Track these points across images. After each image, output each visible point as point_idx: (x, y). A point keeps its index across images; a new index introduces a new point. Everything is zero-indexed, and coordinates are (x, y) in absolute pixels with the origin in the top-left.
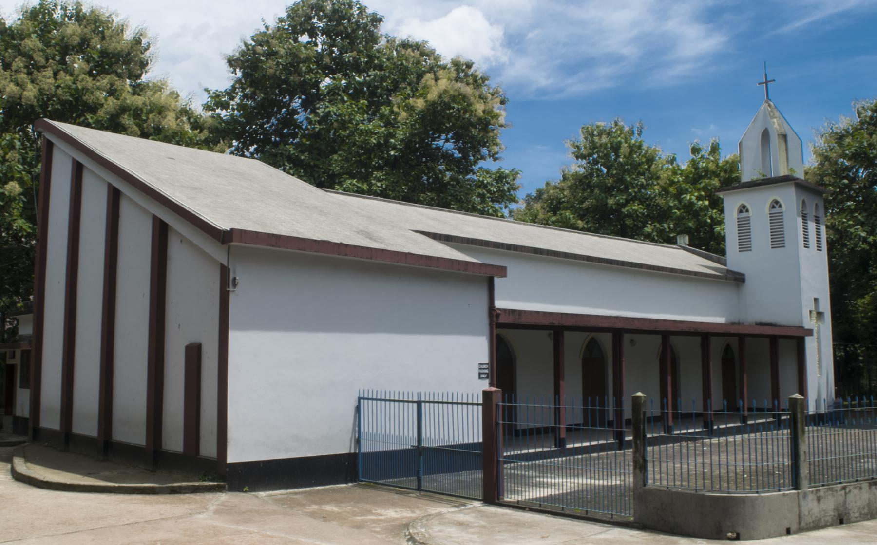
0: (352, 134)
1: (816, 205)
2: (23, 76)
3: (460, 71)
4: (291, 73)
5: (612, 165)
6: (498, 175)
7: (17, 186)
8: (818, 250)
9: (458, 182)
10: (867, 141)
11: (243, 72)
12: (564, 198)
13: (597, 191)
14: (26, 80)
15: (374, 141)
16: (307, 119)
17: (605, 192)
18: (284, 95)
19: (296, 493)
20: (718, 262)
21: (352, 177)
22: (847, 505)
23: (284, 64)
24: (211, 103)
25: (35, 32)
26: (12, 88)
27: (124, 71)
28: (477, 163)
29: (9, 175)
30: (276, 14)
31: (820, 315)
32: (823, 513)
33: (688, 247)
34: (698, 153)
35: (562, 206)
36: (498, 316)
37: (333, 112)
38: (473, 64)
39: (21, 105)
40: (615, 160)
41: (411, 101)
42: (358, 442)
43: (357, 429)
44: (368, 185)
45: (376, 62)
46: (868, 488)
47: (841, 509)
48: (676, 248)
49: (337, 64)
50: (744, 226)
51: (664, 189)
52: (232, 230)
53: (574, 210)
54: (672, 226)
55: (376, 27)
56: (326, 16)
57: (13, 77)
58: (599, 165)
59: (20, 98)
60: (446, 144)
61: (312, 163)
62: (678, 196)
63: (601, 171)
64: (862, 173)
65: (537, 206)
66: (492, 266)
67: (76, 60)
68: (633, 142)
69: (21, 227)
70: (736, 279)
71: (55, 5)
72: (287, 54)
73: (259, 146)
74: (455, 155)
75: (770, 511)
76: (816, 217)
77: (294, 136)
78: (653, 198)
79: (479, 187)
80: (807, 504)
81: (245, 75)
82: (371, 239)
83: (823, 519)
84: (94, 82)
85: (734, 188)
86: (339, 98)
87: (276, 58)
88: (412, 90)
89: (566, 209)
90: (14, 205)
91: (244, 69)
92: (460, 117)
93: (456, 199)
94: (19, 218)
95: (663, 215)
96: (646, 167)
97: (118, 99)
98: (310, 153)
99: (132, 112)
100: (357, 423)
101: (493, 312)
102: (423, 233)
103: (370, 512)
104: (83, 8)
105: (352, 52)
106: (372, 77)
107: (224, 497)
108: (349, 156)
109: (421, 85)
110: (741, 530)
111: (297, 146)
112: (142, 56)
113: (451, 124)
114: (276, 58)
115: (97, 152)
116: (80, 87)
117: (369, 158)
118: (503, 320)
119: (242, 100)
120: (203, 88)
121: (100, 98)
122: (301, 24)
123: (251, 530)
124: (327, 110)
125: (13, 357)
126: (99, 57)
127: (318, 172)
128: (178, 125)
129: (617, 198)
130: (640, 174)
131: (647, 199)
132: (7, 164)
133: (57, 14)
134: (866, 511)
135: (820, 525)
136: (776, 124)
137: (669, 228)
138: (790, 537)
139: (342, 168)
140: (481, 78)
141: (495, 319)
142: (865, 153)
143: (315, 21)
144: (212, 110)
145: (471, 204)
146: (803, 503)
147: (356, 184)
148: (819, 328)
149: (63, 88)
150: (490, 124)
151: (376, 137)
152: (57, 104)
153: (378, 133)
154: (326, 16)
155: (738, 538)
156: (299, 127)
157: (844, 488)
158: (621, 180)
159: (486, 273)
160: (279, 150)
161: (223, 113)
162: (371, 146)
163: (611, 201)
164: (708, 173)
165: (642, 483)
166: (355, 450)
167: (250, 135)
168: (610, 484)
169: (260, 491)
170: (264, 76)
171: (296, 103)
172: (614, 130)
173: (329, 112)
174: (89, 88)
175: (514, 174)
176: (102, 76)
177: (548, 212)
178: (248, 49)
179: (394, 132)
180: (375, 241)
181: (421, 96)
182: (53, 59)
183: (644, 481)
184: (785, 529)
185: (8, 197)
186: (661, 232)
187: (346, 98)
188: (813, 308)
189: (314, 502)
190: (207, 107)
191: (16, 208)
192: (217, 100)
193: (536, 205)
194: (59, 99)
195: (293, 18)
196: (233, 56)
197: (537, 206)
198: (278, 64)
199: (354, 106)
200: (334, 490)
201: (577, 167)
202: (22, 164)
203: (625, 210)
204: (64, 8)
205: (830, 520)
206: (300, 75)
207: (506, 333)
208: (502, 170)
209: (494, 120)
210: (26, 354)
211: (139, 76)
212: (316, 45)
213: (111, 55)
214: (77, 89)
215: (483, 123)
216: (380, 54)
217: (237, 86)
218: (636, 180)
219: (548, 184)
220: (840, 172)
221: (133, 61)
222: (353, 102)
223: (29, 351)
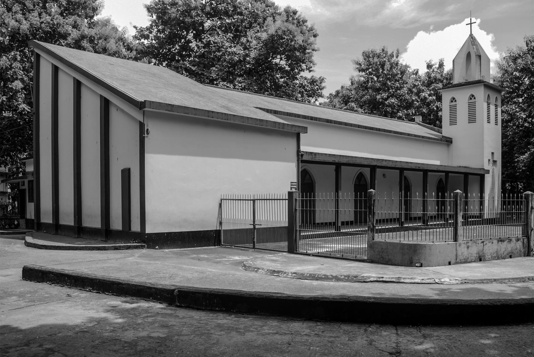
0: (224, 54)
1: (496, 98)
2: (19, 16)
3: (289, 16)
4: (186, 16)
5: (380, 75)
6: (311, 80)
7: (20, 83)
8: (496, 124)
10: (530, 61)
11: (156, 16)
12: (352, 95)
14: (21, 18)
16: (197, 45)
17: (375, 92)
18: (182, 31)
19: (185, 250)
20: (438, 132)
21: (224, 81)
22: (484, 251)
23: (182, 10)
24: (138, 35)
26: (13, 23)
27: (83, 13)
28: (300, 74)
31: (495, 162)
32: (470, 255)
33: (421, 123)
35: (350, 100)
36: (302, 155)
37: (212, 41)
38: (297, 12)
39: (19, 34)
40: (382, 72)
41: (259, 34)
42: (221, 223)
43: (220, 216)
44: (233, 85)
45: (239, 10)
46: (497, 243)
48: (414, 124)
49: (215, 12)
50: (453, 110)
51: (410, 91)
52: (145, 101)
53: (357, 103)
54: (414, 112)
57: (13, 17)
58: (372, 76)
59: (19, 29)
61: (200, 72)
62: (418, 94)
63: (374, 79)
64: (527, 81)
65: (336, 100)
67: (53, 6)
68: (393, 61)
69: (24, 109)
70: (447, 141)
72: (183, 5)
73: (169, 62)
74: (286, 69)
75: (440, 252)
76: (495, 105)
77: (190, 56)
78: (404, 95)
79: (300, 87)
80: (461, 250)
81: (158, 18)
82: (229, 110)
83: (470, 258)
84: (64, 20)
86: (216, 32)
87: (177, 7)
88: (260, 28)
89: (352, 101)
90: (19, 95)
91: (157, 14)
92: (288, 44)
93: (286, 94)
94: (23, 103)
95: (409, 105)
96: (400, 76)
97: (80, 31)
98: (199, 66)
99: (88, 38)
100: (220, 213)
102: (260, 109)
103: (225, 257)
105: (223, 3)
106: (236, 19)
109: (265, 24)
110: (422, 262)
111: (191, 62)
112: (94, 4)
113: (283, 48)
114: (177, 7)
116: (56, 23)
117: (234, 69)
118: (305, 158)
119: (157, 34)
120: (132, 26)
121: (69, 30)
123: (157, 263)
125: (24, 185)
127: (203, 78)
128: (117, 47)
129: (382, 95)
130: (396, 81)
131: (400, 96)
132: (13, 70)
134: (495, 255)
135: (468, 261)
136: (475, 49)
137: (412, 113)
138: (450, 266)
140: (302, 21)
142: (529, 68)
144: (138, 40)
145: (295, 97)
146: (458, 248)
147: (226, 85)
148: (493, 169)
149: (45, 23)
151: (238, 56)
152: (42, 33)
153: (239, 54)
155: (421, 266)
156: (192, 51)
157: (483, 242)
158: (385, 84)
159: (295, 130)
160: (180, 64)
161: (146, 42)
162: (235, 62)
163: (378, 97)
164: (436, 80)
165: (372, 239)
166: (219, 228)
168: (362, 247)
169: (165, 249)
170: (170, 18)
171: (190, 36)
172: (382, 54)
173: (210, 41)
174: (61, 23)
175: (322, 80)
176: (69, 16)
177: (342, 103)
179: (249, 53)
180: (231, 111)
181: (265, 31)
182: (38, 5)
183: (373, 237)
184: (448, 262)
185: (14, 90)
186: (407, 115)
187: (220, 33)
189: (195, 254)
190: (135, 37)
191: (21, 97)
192: (142, 33)
193: (335, 100)
194: (43, 30)
196: (151, 5)
197: (336, 100)
198: (178, 10)
199: (224, 37)
201: (360, 77)
202: (22, 71)
203: (386, 102)
205: (474, 259)
206: (192, 18)
207: (310, 168)
208: (314, 78)
209: (309, 46)
210: (31, 182)
211: (92, 17)
213: (74, 3)
214: (54, 24)
215: (302, 48)
216: (241, 5)
217: (154, 24)
218: (394, 84)
219: (342, 87)
220: (514, 80)
221: (88, 7)
222: (224, 35)
223: (33, 181)
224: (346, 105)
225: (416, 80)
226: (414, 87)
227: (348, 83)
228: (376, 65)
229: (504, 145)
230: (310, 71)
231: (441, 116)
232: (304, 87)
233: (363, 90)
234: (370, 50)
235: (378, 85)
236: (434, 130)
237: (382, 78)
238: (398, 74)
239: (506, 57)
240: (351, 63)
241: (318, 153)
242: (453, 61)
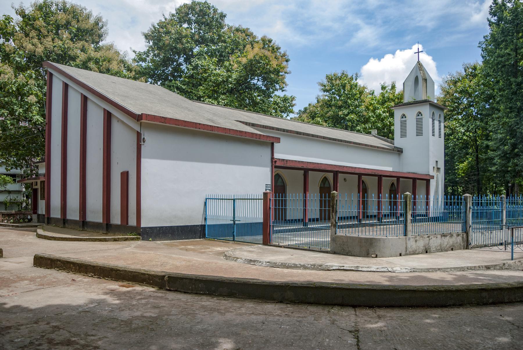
0: (209, 75)
2: (35, 41)
4: (178, 43)
5: (342, 95)
7: (34, 98)
9: (264, 102)
13: (333, 108)
15: (220, 79)
19: (175, 242)
20: (391, 143)
25: (41, 17)
26: (30, 47)
29: (30, 92)
30: (170, 12)
31: (438, 169)
34: (385, 89)
36: (275, 162)
38: (272, 40)
39: (35, 56)
40: (344, 92)
41: (240, 59)
42: (205, 219)
47: (427, 246)
49: (202, 40)
50: (403, 125)
51: (367, 108)
54: (370, 126)
55: (223, 20)
56: (196, 13)
59: (35, 52)
60: (258, 82)
61: (189, 91)
62: (374, 111)
65: (304, 116)
66: (273, 137)
69: (38, 119)
70: (398, 151)
71: (52, 3)
74: (263, 88)
75: (392, 245)
77: (180, 77)
79: (274, 104)
81: (154, 44)
85: (399, 106)
88: (241, 53)
89: (318, 117)
90: (33, 107)
92: (264, 68)
95: (366, 121)
101: (273, 160)
102: (240, 122)
104: (67, 5)
107: (139, 242)
108: (208, 87)
109: (245, 50)
111: (181, 82)
112: (100, 32)
115: (75, 77)
117: (219, 88)
122: (183, 17)
124: (196, 63)
126: (76, 31)
130: (355, 99)
131: (359, 112)
132: (29, 86)
133: (54, 8)
134: (439, 248)
137: (369, 127)
139: (204, 93)
141: (274, 163)
142: (467, 90)
143: (191, 16)
144: (137, 62)
146: (408, 241)
148: (437, 175)
150: (280, 72)
152: (54, 56)
153: (223, 75)
154: (196, 13)
155: (376, 257)
157: (429, 237)
158: (346, 102)
161: (144, 64)
163: (340, 113)
167: (158, 76)
171: (181, 60)
173: (198, 64)
175: (293, 99)
178: (156, 30)
181: (245, 56)
187: (206, 57)
188: (435, 166)
189: (183, 245)
190: (134, 60)
193: (303, 115)
194: (56, 53)
195: (179, 14)
196: (148, 34)
197: (304, 116)
200: (193, 241)
201: (325, 96)
203: (347, 118)
204: (57, 5)
206: (182, 44)
210: (42, 183)
211: (98, 43)
212: (192, 29)
214: (65, 48)
217: (150, 50)
219: (310, 105)
223: (44, 181)
224: (313, 119)
225: (372, 99)
226: (370, 106)
227: (315, 102)
228: (338, 86)
229: (446, 155)
230: (283, 91)
231: (393, 130)
232: (277, 104)
233: (327, 107)
234: (333, 74)
235: (340, 103)
236: (387, 142)
237: (344, 97)
238: (357, 94)
240: (317, 85)
241: (289, 160)
242: (404, 84)
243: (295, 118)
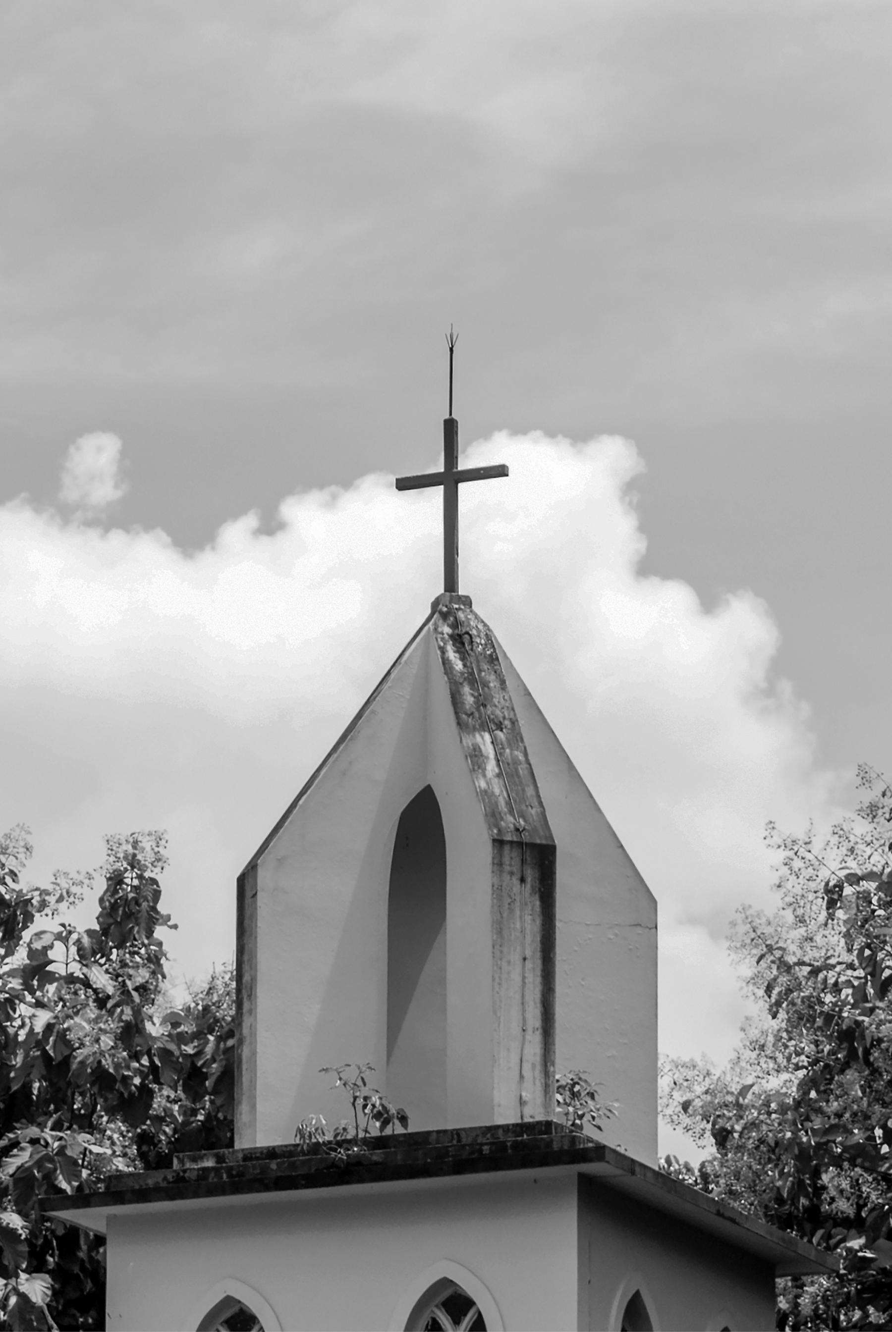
42: (522, 1117)
136: (491, 767)
239: (853, 879)
243: (88, 1060)
